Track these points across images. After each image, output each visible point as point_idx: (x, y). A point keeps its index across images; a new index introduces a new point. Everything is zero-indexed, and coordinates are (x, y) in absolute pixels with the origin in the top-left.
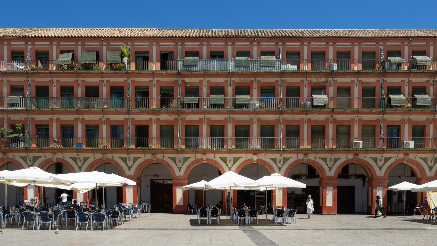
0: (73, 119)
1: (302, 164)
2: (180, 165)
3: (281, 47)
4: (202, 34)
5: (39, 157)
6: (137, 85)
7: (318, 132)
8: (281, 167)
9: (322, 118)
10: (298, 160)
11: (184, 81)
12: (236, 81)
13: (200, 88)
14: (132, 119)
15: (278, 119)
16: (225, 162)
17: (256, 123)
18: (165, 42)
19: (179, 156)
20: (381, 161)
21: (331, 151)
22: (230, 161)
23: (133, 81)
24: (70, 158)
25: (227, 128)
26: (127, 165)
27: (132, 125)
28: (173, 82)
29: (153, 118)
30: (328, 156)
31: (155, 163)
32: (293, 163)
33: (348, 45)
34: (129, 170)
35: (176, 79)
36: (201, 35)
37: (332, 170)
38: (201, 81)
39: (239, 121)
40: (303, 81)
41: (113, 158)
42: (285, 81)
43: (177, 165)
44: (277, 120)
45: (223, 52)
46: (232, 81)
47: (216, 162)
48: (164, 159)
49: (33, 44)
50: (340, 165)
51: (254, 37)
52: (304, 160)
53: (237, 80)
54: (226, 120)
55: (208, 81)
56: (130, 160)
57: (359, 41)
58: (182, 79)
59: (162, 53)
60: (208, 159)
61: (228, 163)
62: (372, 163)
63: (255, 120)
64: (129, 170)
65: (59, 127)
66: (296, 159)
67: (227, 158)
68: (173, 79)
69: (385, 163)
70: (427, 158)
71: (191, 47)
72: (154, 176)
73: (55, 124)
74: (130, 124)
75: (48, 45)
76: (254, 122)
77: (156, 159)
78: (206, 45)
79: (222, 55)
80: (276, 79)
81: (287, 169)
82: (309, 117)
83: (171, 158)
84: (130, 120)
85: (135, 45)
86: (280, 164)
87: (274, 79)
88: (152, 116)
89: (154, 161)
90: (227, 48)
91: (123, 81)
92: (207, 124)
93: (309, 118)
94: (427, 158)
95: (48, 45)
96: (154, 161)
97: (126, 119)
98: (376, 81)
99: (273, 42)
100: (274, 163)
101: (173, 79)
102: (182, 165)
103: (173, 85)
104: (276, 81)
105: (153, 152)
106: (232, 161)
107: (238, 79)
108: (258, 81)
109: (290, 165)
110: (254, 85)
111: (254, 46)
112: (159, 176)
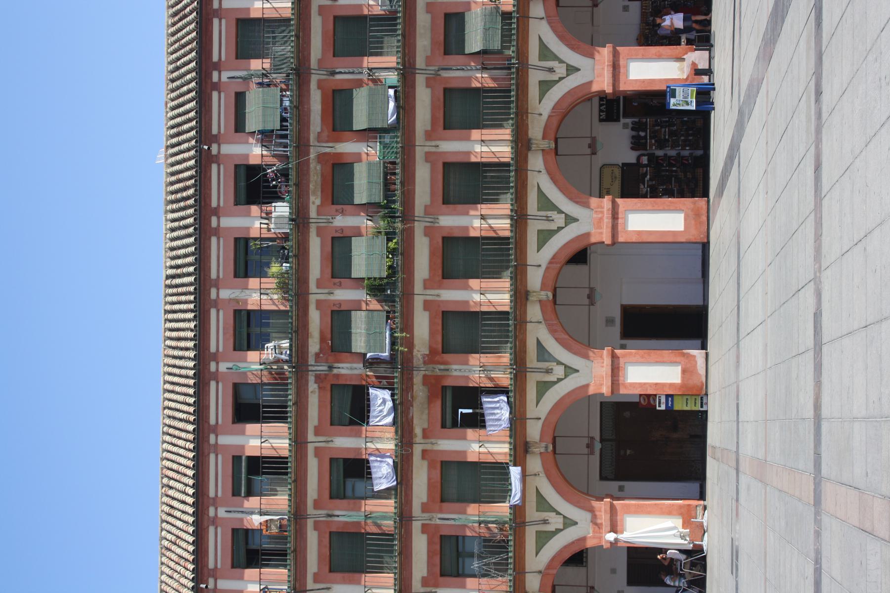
0: (425, 463)
1: (556, 154)
2: (561, 70)
3: (225, 76)
8: (568, 65)
12: (318, 202)
13: (335, 308)
14: (423, 511)
15: (427, 79)
16: (551, 233)
17: (438, 143)
18: (208, 407)
20: (551, 70)
21: (519, 219)
22: (548, 219)
25: (451, 228)
26: (558, 531)
27: (441, 511)
28: (320, 388)
32: (555, 31)
33: (220, 25)
34: (576, 523)
35: (311, 379)
37: (574, 215)
40: (317, 449)
41: (540, 572)
42: (320, 61)
43: (559, 380)
45: (237, 240)
46: (319, 213)
47: (550, 263)
48: (543, 418)
51: (200, 151)
53: (315, 201)
55: (319, 286)
56: (545, 522)
57: (205, 524)
60: (544, 287)
61: (553, 227)
62: (556, 94)
63: (432, 294)
64: (576, 523)
66: (544, 23)
67: (539, 379)
68: (313, 386)
70: (537, 511)
71: (224, 334)
73: (440, 442)
74: (437, 519)
75: (216, 528)
76: (433, 149)
77: (541, 440)
78: (217, 363)
80: (313, 85)
81: (572, 48)
82: (418, 287)
83: (540, 395)
84: (426, 515)
85: (216, 567)
88: (416, 526)
89: (546, 447)
90: (226, 155)
91: (316, 534)
92: (440, 287)
93: (423, 208)
94: (537, 511)
95: (216, 528)
96: (546, 447)
97: (425, 529)
99: (210, 99)
100: (555, 88)
101: (313, 386)
102: (559, 363)
103: (329, 387)
104: (319, 87)
105: (520, 450)
106: (549, 213)
107: (312, 198)
109: (561, 38)
111: (222, 225)
112: (592, 438)
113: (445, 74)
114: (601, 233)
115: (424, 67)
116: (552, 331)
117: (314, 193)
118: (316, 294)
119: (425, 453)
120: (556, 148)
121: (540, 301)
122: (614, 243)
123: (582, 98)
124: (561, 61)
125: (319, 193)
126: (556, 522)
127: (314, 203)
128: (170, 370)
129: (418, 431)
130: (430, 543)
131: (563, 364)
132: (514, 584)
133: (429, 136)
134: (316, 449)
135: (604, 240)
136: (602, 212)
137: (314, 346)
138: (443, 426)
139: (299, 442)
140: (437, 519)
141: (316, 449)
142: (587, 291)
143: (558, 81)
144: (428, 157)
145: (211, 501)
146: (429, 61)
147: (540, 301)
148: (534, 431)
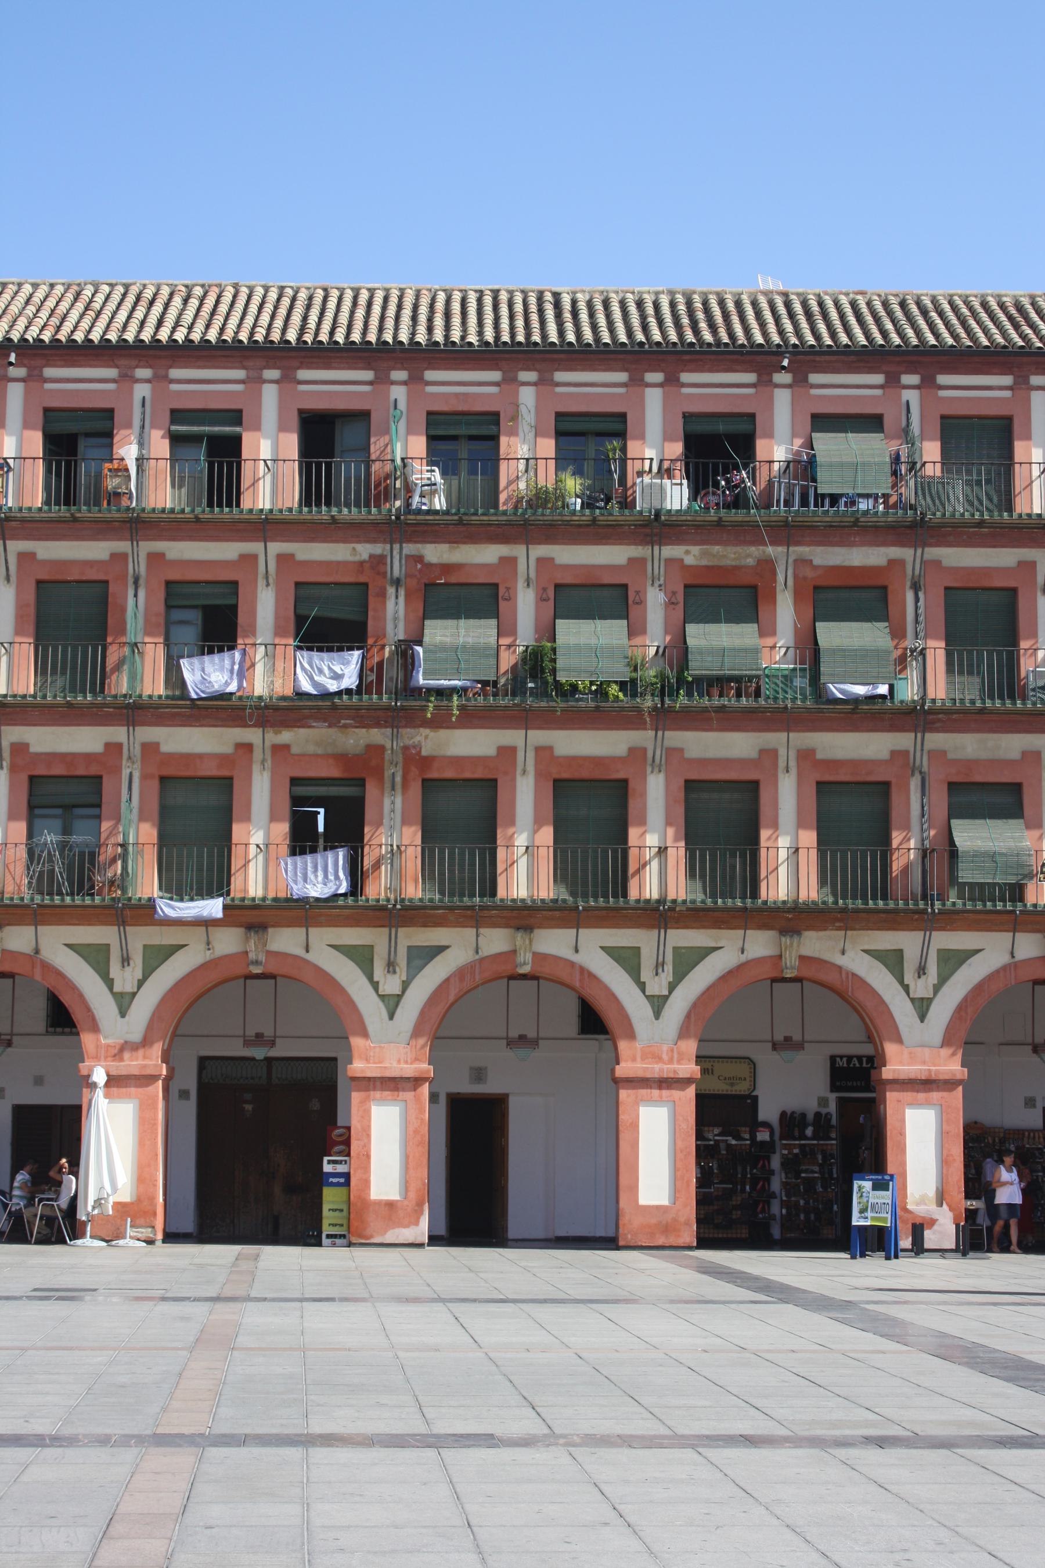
1: (774, 980)
2: (921, 988)
4: (252, 334)
5: (705, 952)
6: (175, 575)
7: (592, 817)
9: (737, 745)
10: (1013, 967)
11: (419, 559)
12: (689, 560)
13: (502, 591)
16: (634, 970)
19: (925, 946)
20: (921, 971)
22: (659, 966)
23: (156, 559)
24: (978, 951)
25: (643, 794)
26: (109, 983)
27: (144, 777)
28: (361, 563)
29: (520, 744)
30: (643, 939)
31: (257, 977)
35: (378, 549)
36: (95, 336)
38: (510, 562)
39: (704, 762)
41: (37, 951)
42: (937, 563)
43: (375, 986)
44: (898, 755)
45: (622, 417)
46: (669, 561)
47: (582, 969)
49: (160, 379)
50: (73, 988)
51: (778, 352)
52: (252, 956)
53: (691, 554)
54: (637, 754)
56: (126, 961)
58: (409, 549)
59: (304, 415)
60: (540, 958)
61: (646, 975)
63: (526, 760)
65: (811, 791)
66: (1004, 959)
68: (364, 550)
69: (943, 980)
71: (457, 395)
72: (247, 1043)
73: (266, 776)
74: (131, 770)
76: (782, 763)
77: (269, 953)
79: (617, 427)
80: (895, 552)
81: (961, 1009)
82: (539, 737)
83: (613, 953)
84: (137, 751)
86: (921, 982)
87: (883, 550)
88: (118, 733)
92: (539, 775)
94: (145, 946)
96: (257, 963)
98: (631, 560)
101: (364, 550)
102: (405, 985)
103: (362, 579)
106: (669, 968)
107: (695, 550)
108: (802, 562)
109: (978, 989)
110: (780, 578)
111: (777, 392)
112: (272, 1043)
113: (915, 783)
114: (634, 1059)
115: (926, 748)
116: (461, 973)
117: (704, 554)
118: (526, 556)
119: (246, 748)
120: (784, 980)
121: (514, 952)
122: (618, 1082)
123: (873, 1025)
124: (141, 983)
125: (704, 562)
126: (125, 979)
127: (687, 552)
128: (394, 301)
129: (286, 736)
130: (89, 758)
131: (404, 991)
132: (16, 906)
133: (806, 756)
134: (254, 557)
135: (623, 1064)
136: (671, 1061)
137: (435, 553)
138: (294, 781)
139: (267, 526)
140: (131, 770)
141: (254, 557)
142: (531, 1034)
143: (901, 981)
144: (769, 755)
145: (162, 372)
146: (938, 755)
147: (514, 952)
148: (286, 940)
